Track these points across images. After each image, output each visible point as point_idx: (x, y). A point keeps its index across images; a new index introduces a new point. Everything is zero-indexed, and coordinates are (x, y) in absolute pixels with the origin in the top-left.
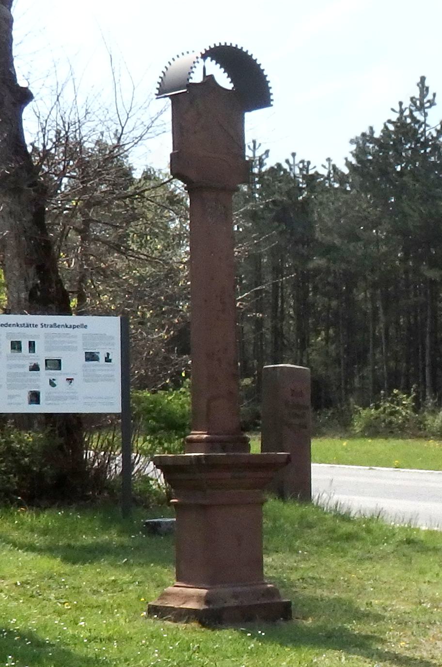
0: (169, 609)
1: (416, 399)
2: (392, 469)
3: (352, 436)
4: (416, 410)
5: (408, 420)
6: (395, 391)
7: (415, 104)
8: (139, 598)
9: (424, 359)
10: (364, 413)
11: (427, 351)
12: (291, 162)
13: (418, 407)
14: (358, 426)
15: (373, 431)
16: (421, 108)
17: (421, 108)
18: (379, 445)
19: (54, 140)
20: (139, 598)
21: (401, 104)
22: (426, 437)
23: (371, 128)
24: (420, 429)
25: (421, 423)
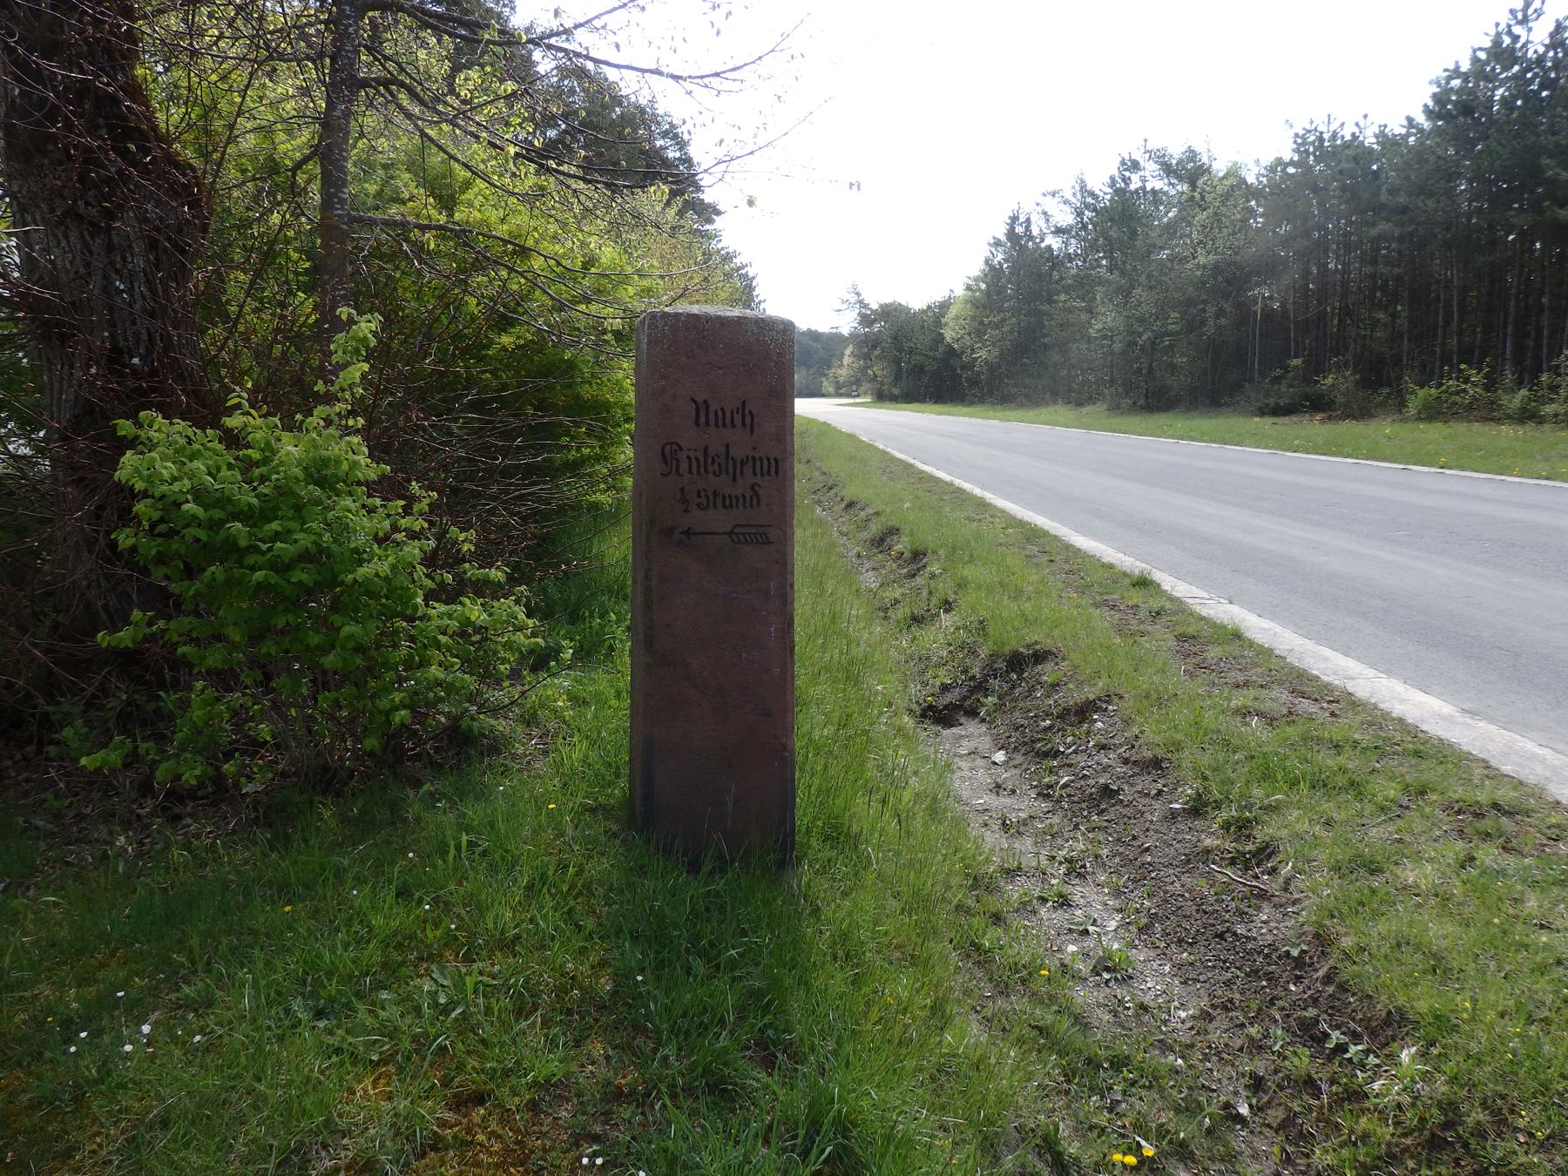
0: (1348, 450)
1: (1486, 376)
2: (1433, 470)
3: (1405, 420)
4: (1487, 388)
5: (1477, 400)
6: (1463, 366)
7: (1516, 18)
8: (977, 1012)
9: (1505, 327)
10: (1422, 393)
11: (1511, 319)
12: (1362, 125)
13: (1491, 384)
14: (1413, 405)
15: (1432, 413)
16: (1524, 21)
17: (1524, 21)
18: (1434, 432)
19: (1152, 954)
20: (977, 1012)
21: (1497, 25)
22: (1498, 421)
23: (1457, 62)
24: (1494, 410)
25: (1493, 403)
